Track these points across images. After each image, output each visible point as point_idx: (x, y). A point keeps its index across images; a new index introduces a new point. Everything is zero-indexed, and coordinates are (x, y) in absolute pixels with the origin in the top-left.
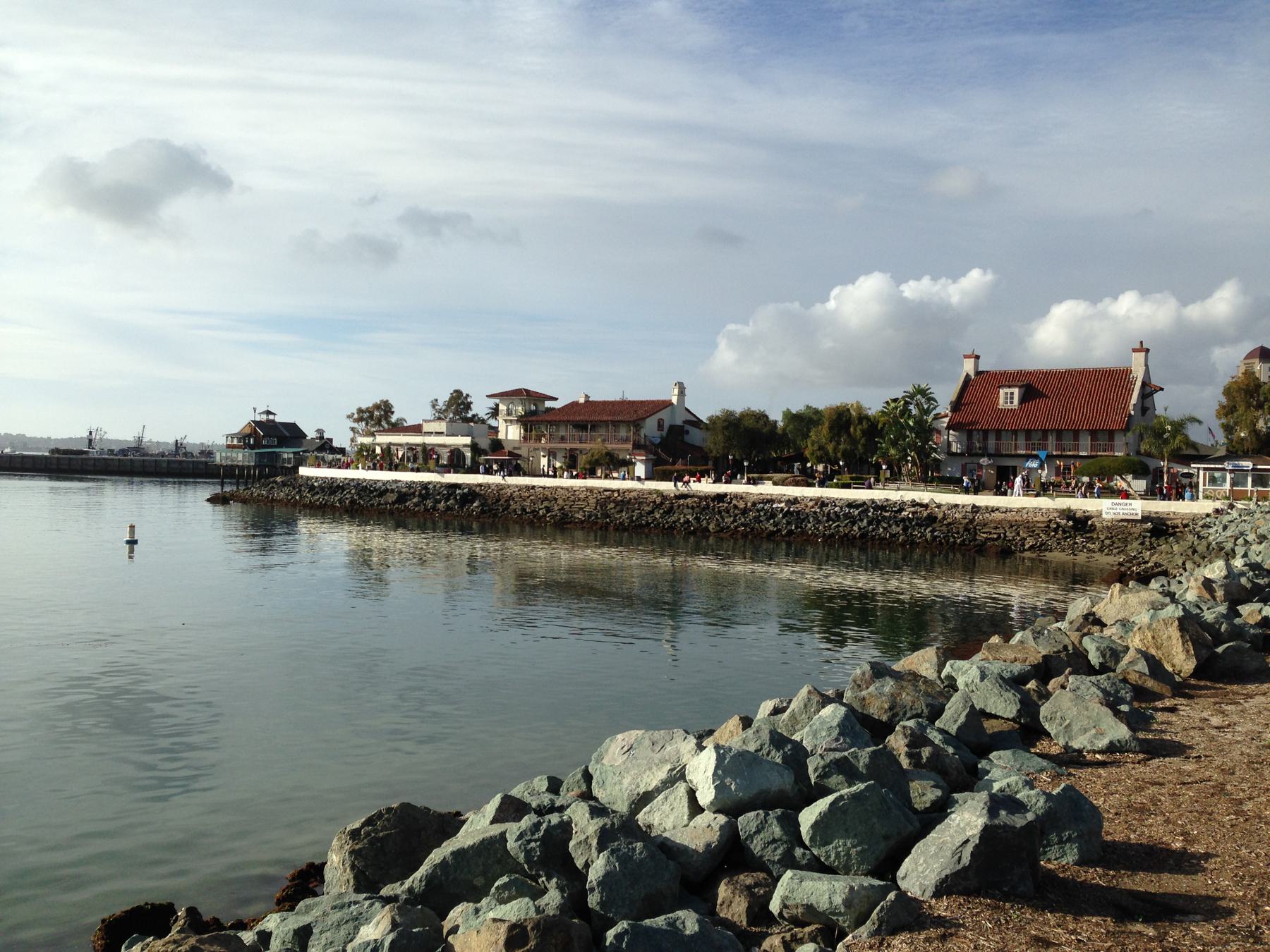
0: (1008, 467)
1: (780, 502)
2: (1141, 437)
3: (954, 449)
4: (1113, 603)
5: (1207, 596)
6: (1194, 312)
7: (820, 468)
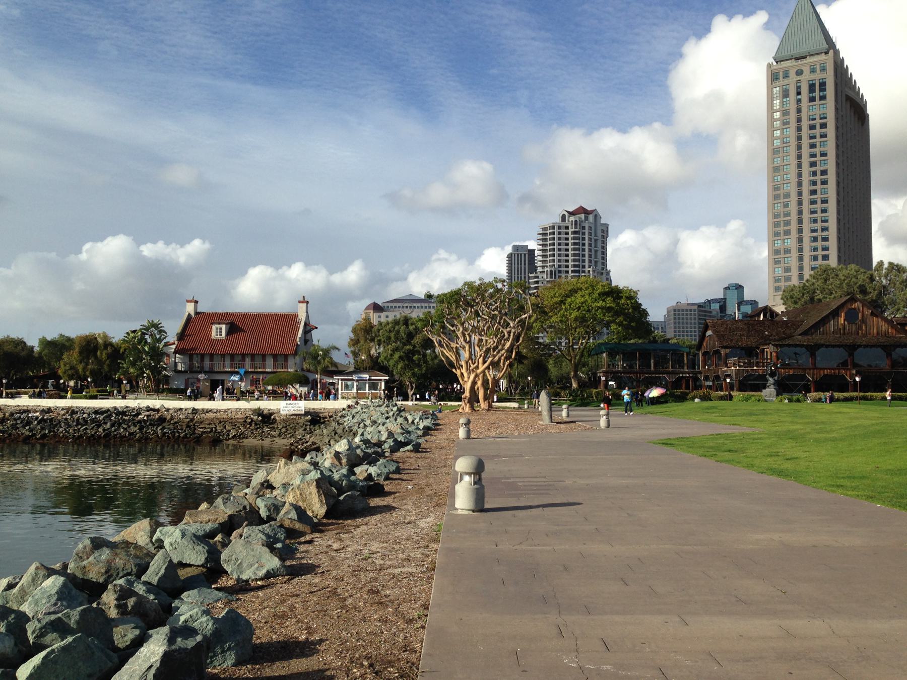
0: (218, 380)
1: (35, 412)
2: (304, 359)
3: (179, 368)
4: (284, 472)
5: (337, 463)
6: (337, 278)
7: (72, 383)
